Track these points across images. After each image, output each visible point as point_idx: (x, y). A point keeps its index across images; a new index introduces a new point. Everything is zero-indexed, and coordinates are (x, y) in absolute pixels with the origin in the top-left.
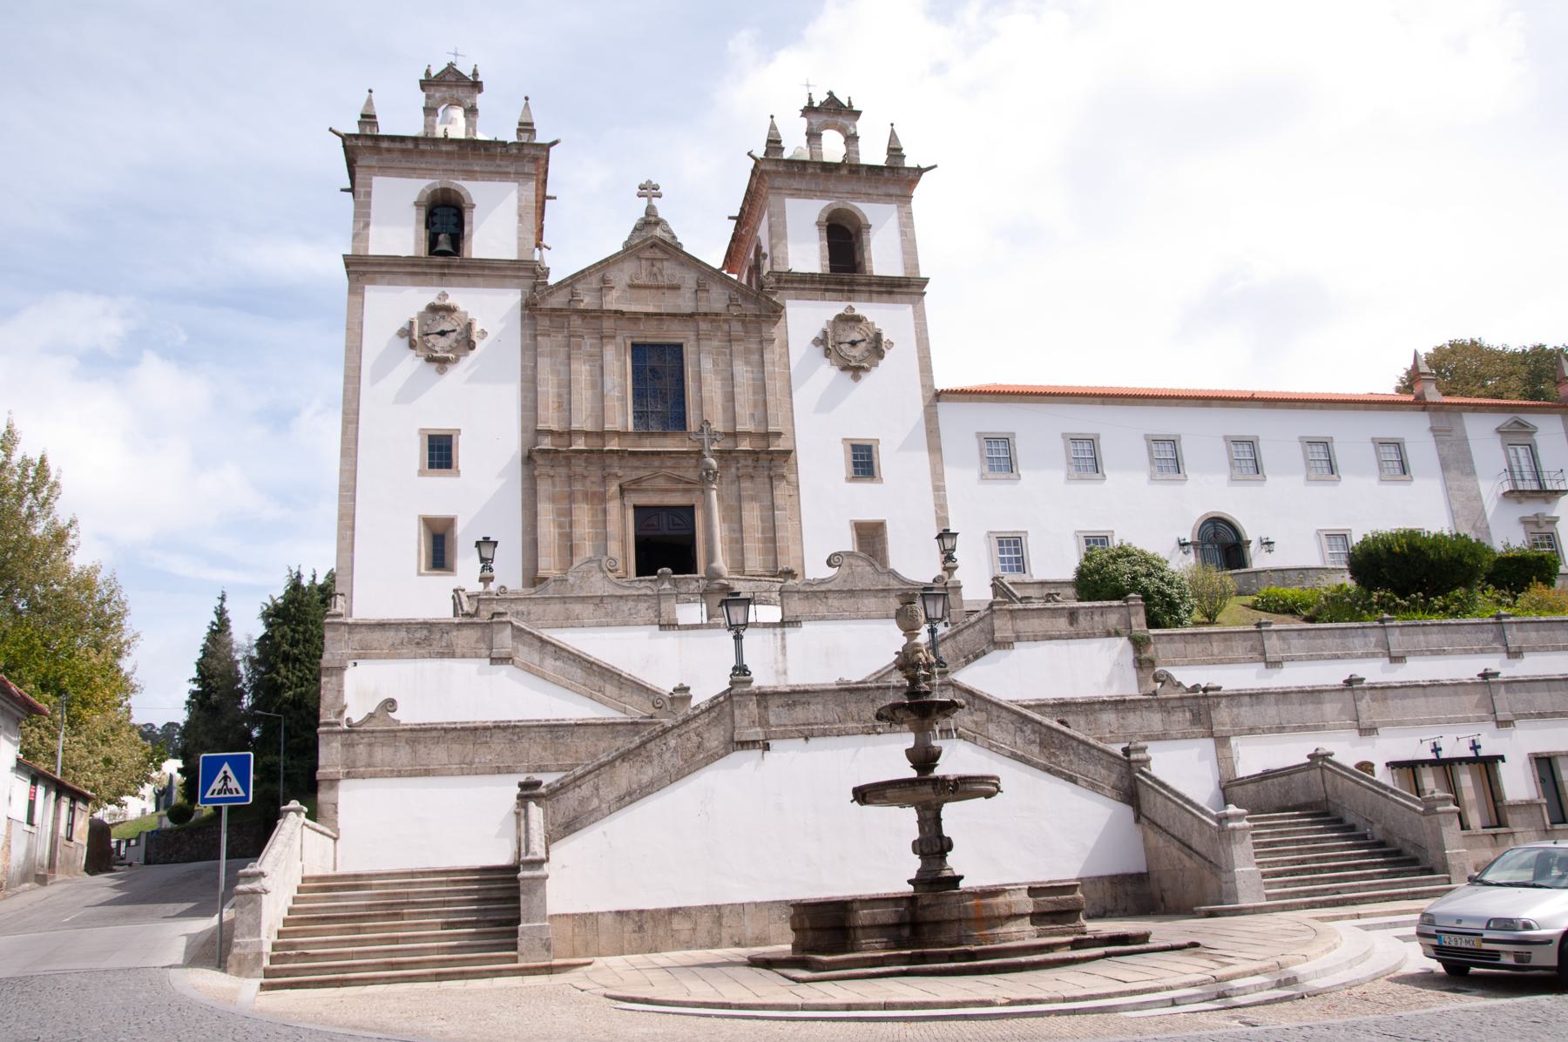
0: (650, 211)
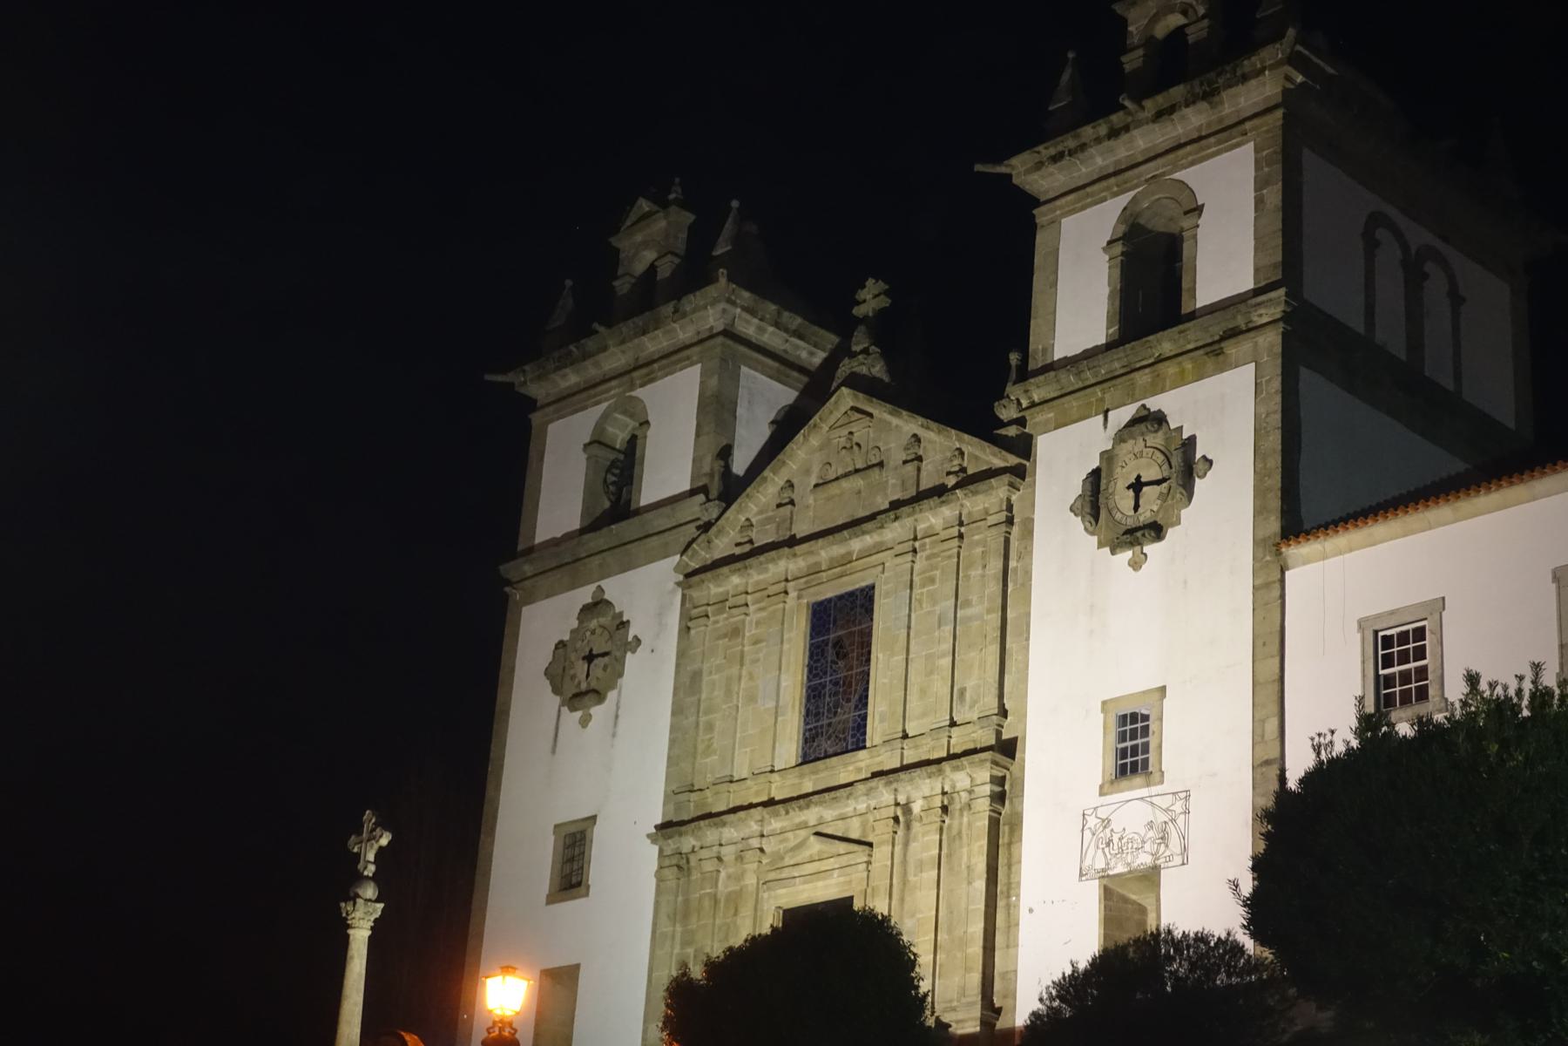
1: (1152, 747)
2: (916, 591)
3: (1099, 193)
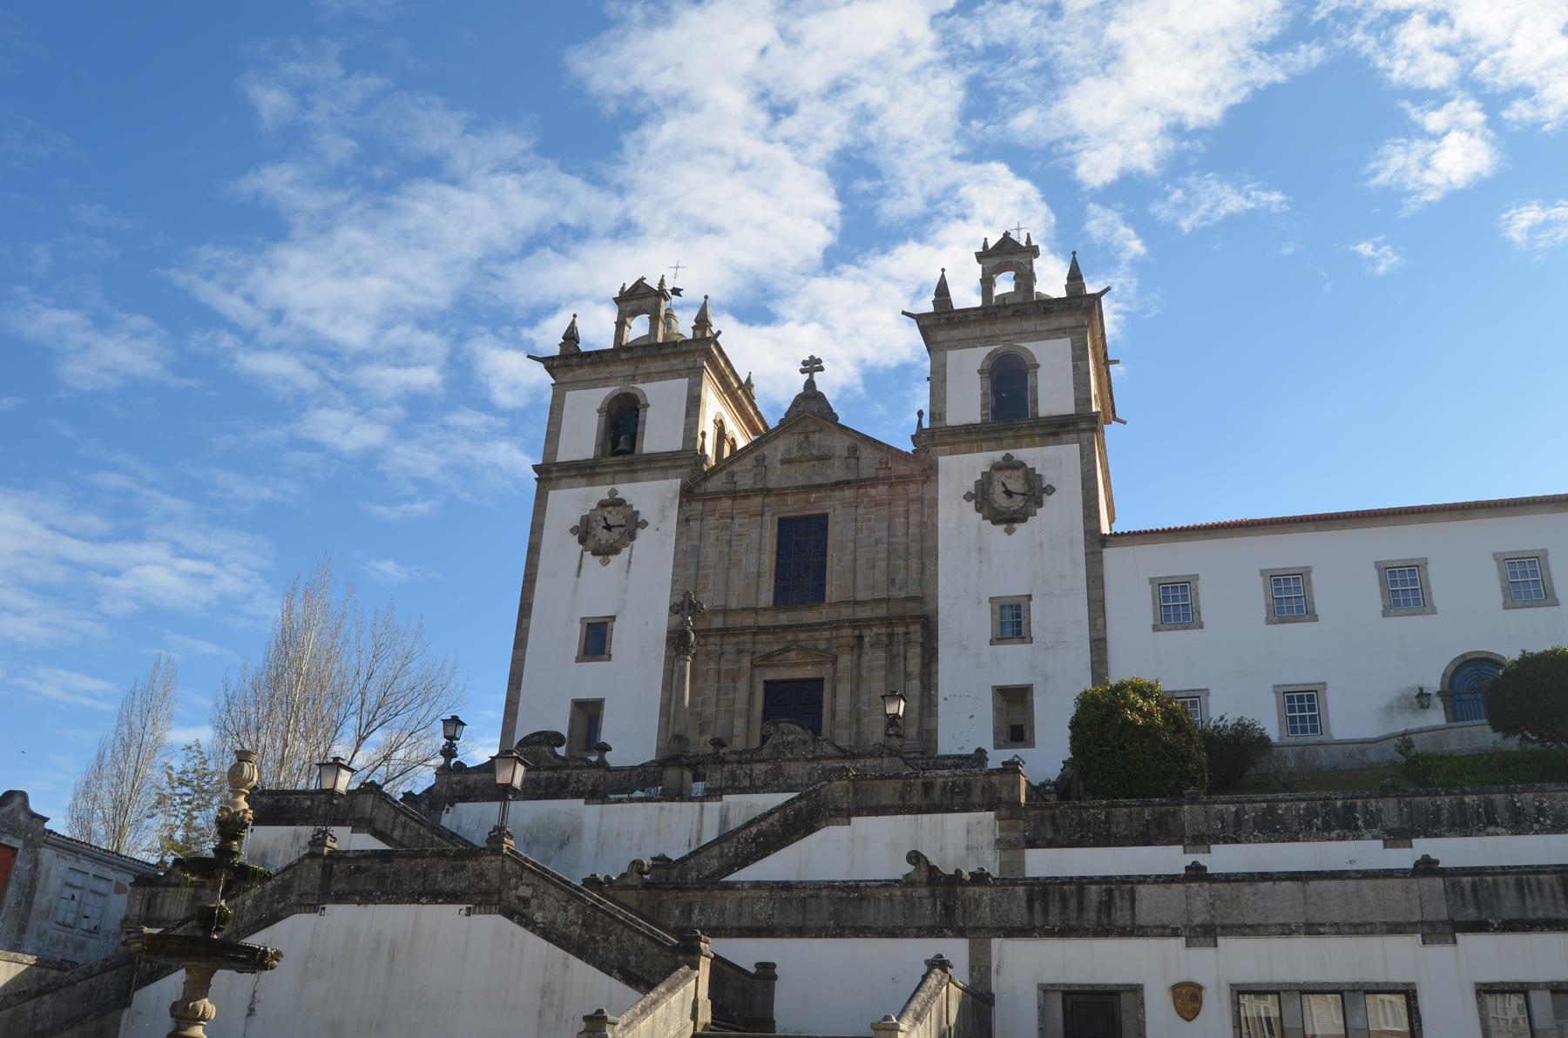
0: (810, 384)
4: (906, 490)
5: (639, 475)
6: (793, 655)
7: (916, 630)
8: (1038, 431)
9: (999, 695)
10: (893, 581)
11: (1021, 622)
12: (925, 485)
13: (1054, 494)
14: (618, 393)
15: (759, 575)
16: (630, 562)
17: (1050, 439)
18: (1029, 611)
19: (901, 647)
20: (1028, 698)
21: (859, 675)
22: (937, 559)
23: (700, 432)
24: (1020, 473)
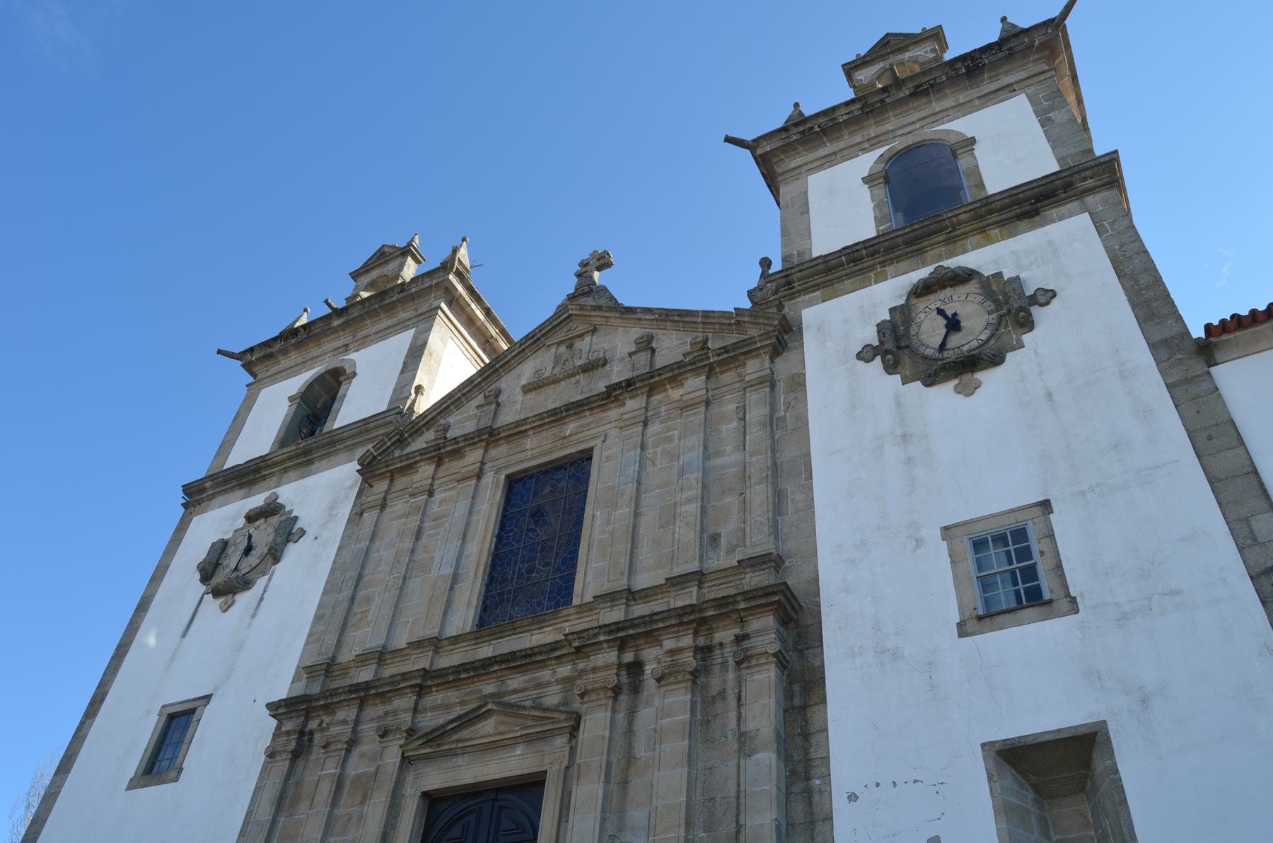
1: (1041, 570)
2: (650, 452)
3: (607, 403)
4: (740, 375)
5: (315, 466)
6: (487, 727)
7: (764, 630)
8: (994, 218)
9: (1009, 772)
10: (715, 538)
11: (1034, 566)
12: (777, 360)
13: (1054, 302)
14: (323, 371)
15: (455, 578)
16: (262, 599)
17: (1022, 224)
18: (1051, 536)
19: (731, 676)
20: (1099, 766)
21: (630, 758)
22: (810, 477)
23: (415, 384)
24: (972, 287)
